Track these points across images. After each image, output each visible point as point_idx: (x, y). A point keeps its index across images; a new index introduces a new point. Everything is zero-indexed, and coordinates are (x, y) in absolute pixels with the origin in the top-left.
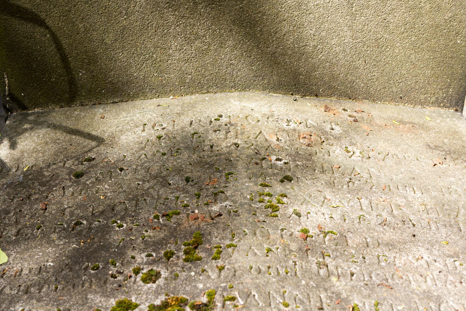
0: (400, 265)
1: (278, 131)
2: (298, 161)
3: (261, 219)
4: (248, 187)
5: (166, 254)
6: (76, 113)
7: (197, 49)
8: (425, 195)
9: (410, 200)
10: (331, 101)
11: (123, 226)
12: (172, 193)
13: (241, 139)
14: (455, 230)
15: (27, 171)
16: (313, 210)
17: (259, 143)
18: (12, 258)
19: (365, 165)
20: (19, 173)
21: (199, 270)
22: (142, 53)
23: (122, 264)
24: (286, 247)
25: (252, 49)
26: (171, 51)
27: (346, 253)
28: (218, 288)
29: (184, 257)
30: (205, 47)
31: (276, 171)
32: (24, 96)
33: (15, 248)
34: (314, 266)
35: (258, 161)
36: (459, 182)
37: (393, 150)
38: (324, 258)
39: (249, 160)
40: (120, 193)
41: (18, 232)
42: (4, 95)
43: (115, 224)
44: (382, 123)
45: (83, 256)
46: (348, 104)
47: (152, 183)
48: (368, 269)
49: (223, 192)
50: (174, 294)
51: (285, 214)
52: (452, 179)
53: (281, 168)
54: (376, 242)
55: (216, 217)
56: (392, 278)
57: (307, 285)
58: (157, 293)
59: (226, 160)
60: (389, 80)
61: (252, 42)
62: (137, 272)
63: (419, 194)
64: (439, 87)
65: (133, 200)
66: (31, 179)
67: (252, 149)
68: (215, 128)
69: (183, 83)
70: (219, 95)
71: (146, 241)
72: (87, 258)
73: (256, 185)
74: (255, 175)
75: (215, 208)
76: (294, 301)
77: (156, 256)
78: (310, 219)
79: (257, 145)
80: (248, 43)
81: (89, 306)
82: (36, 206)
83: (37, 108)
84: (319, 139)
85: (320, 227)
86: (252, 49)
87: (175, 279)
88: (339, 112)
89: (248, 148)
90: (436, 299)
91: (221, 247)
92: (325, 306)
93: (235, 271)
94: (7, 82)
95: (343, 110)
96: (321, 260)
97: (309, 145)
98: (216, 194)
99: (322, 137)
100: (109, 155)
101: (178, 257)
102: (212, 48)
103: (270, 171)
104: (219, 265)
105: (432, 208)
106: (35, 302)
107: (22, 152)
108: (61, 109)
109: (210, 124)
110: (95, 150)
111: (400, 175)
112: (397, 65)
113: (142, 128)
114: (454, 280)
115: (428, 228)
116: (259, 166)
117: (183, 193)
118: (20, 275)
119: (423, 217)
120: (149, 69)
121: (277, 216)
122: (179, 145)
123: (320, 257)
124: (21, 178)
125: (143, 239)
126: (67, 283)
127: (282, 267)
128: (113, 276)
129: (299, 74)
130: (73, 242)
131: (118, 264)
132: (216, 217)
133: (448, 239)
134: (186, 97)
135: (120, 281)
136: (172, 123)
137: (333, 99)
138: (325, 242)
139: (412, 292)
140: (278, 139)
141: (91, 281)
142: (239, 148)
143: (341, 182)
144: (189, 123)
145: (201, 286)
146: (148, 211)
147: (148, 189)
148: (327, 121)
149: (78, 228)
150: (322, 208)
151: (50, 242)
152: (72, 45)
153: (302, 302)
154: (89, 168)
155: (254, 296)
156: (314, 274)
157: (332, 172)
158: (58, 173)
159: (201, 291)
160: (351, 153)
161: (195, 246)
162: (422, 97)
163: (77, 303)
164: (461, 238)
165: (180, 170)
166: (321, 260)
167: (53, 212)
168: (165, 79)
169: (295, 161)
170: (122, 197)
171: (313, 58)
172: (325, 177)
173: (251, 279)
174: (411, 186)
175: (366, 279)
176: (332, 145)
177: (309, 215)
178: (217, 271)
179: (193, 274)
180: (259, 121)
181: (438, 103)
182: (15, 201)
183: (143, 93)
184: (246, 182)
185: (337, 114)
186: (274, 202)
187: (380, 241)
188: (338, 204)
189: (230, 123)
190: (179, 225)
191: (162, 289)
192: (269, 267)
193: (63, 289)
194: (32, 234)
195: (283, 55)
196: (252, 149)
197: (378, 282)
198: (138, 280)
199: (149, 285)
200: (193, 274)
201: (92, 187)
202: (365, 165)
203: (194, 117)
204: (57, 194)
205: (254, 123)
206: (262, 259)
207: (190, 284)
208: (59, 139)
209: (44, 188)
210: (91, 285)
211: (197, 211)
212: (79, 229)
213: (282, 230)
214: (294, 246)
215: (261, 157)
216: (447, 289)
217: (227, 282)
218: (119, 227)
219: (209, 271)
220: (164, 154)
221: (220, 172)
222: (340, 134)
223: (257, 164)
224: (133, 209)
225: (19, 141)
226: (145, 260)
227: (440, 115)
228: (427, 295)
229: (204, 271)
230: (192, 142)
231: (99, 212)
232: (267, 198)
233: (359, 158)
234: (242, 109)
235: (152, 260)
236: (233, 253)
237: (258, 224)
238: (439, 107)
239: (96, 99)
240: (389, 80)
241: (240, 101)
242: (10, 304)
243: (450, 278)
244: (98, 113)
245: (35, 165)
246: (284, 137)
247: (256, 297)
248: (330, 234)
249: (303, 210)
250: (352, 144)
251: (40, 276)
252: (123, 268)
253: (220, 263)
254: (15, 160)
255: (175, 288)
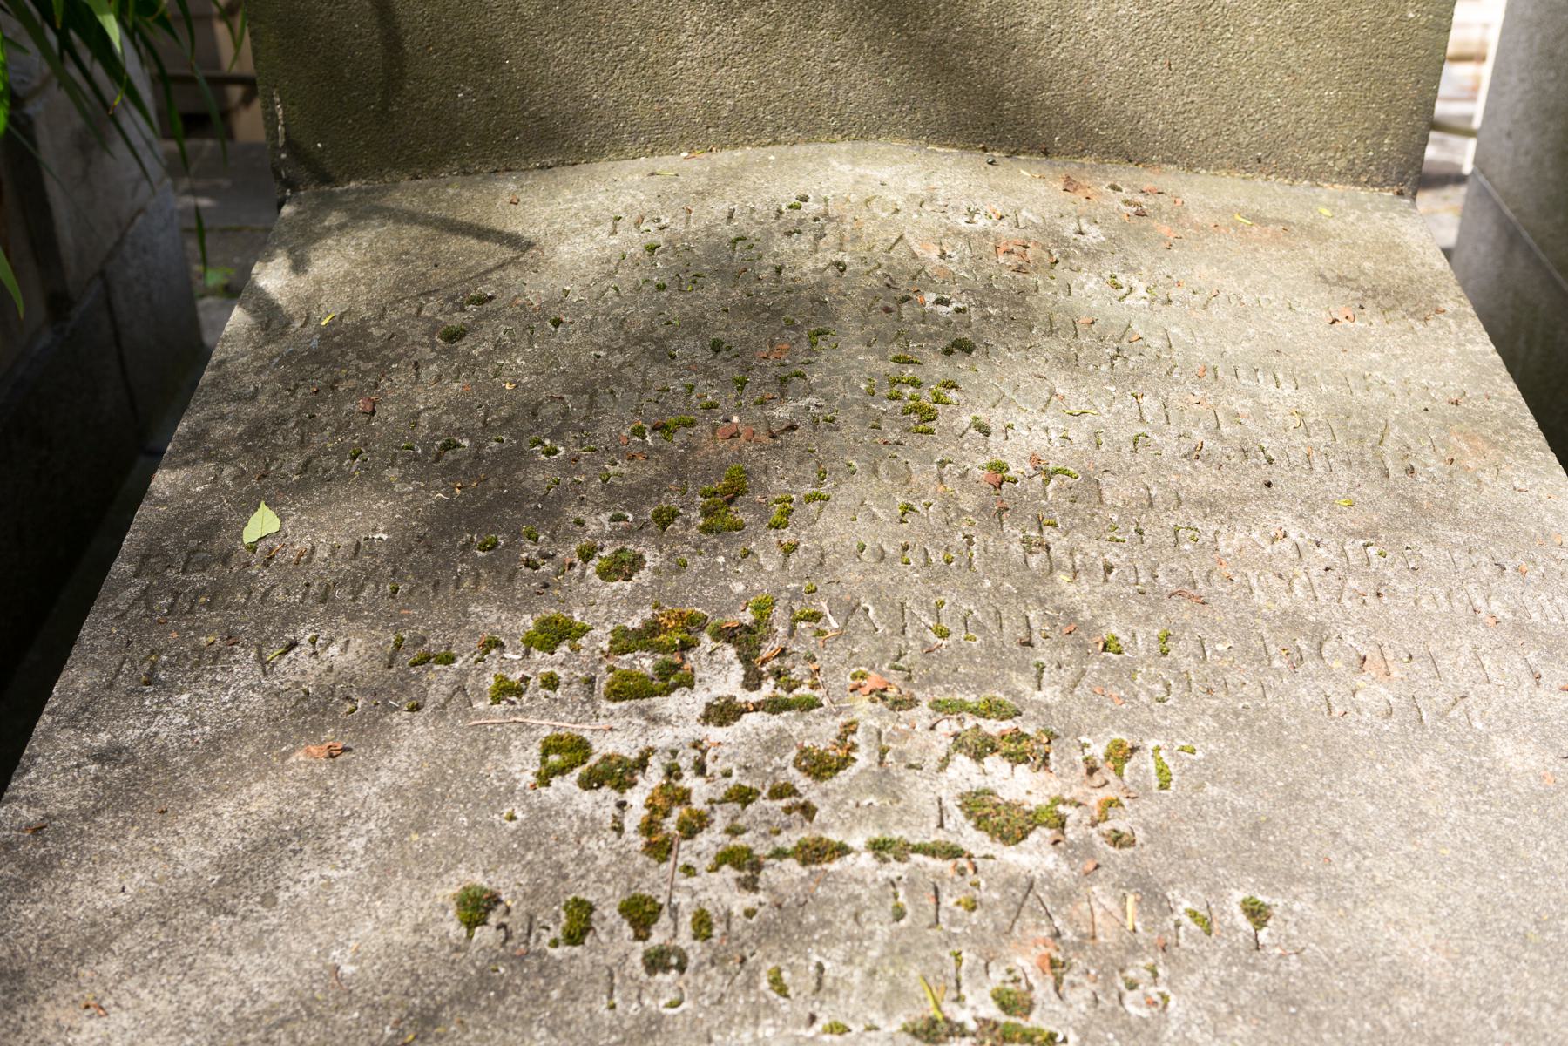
0: (1230, 550)
1: (945, 236)
2: (991, 305)
3: (892, 436)
4: (863, 364)
5: (658, 516)
6: (451, 191)
7: (749, 32)
8: (1303, 391)
9: (1265, 401)
10: (1083, 166)
11: (556, 452)
12: (677, 377)
13: (851, 253)
14: (1374, 474)
15: (329, 325)
16: (1021, 419)
17: (895, 262)
18: (290, 522)
19: (1158, 319)
20: (310, 329)
21: (737, 551)
22: (611, 42)
23: (553, 537)
24: (949, 502)
25: (885, 33)
26: (683, 37)
27: (1096, 519)
28: (780, 591)
29: (701, 522)
30: (768, 27)
31: (935, 328)
32: (324, 148)
33: (299, 500)
34: (1016, 548)
35: (891, 305)
36: (1394, 363)
37: (1230, 285)
38: (1041, 530)
39: (870, 301)
40: (551, 376)
41: (305, 465)
42: (275, 147)
43: (538, 448)
44: (1209, 220)
45: (459, 519)
46: (1126, 175)
47: (629, 354)
48: (1149, 556)
49: (801, 376)
50: (674, 604)
51: (952, 428)
52: (1374, 356)
53: (948, 322)
54: (1172, 497)
55: (782, 432)
56: (1208, 580)
57: (997, 589)
58: (634, 602)
59: (813, 301)
60: (1230, 112)
61: (886, 14)
62: (587, 555)
63: (1288, 389)
64: (1357, 132)
65: (583, 392)
66: (339, 345)
67: (877, 277)
68: (789, 228)
69: (712, 118)
70: (801, 149)
71: (611, 485)
72: (469, 523)
73: (884, 359)
74: (881, 336)
75: (782, 412)
76: (961, 625)
77: (635, 520)
78: (1013, 440)
79: (890, 268)
80: (875, 18)
81: (471, 631)
82: (349, 406)
83: (356, 179)
84: (1046, 256)
85: (1035, 460)
86: (885, 33)
87: (678, 572)
88: (1101, 194)
89: (868, 273)
90: (1314, 631)
91: (791, 501)
92: (1037, 638)
93: (822, 556)
94: (280, 113)
95: (1109, 192)
96: (1034, 534)
97: (1018, 270)
98: (784, 380)
99: (1054, 251)
100: (527, 289)
101: (687, 522)
102: (784, 29)
103: (919, 327)
104: (784, 540)
105: (1318, 423)
106: (344, 621)
107: (319, 282)
108: (415, 183)
109: (778, 218)
110: (494, 276)
111: (1245, 344)
112: (1251, 75)
113: (609, 226)
114: (1361, 590)
115: (1306, 467)
116: (893, 315)
117: (706, 378)
118: (309, 561)
119: (1295, 442)
120: (628, 82)
121: (931, 432)
122: (698, 266)
123: (1032, 528)
124: (315, 342)
125: (604, 481)
126: (421, 578)
127: (938, 547)
128: (529, 563)
129: (1003, 98)
130: (437, 488)
131: (542, 537)
132: (782, 432)
133: (1353, 494)
134: (720, 155)
135: (547, 574)
136: (684, 216)
137: (1087, 161)
138: (1045, 494)
139: (1253, 613)
140: (943, 255)
141: (479, 575)
142: (846, 274)
143: (1096, 358)
144: (725, 216)
145: (739, 587)
146: (619, 417)
147: (620, 367)
148: (1069, 214)
149: (450, 456)
150: (1044, 416)
151: (382, 487)
152: (438, 21)
153: (981, 628)
154: (479, 319)
155: (867, 610)
156: (1016, 564)
157: (1072, 333)
158: (404, 331)
159: (739, 597)
160: (1125, 290)
161: (727, 502)
162: (1314, 158)
163: (444, 624)
164: (1388, 494)
165: (699, 325)
166: (1034, 534)
167: (391, 419)
168: (669, 109)
169: (982, 305)
170: (556, 386)
171: (1037, 57)
172: (1056, 345)
173: (861, 572)
174: (1271, 370)
175: (1142, 581)
176: (1079, 270)
177: (1010, 432)
178: (779, 553)
179: (721, 559)
180: (897, 211)
181: (1353, 175)
182: (300, 394)
183: (615, 143)
184: (859, 352)
185: (1094, 199)
186: (926, 399)
187: (1182, 495)
188: (1084, 407)
189: (826, 215)
190: (693, 449)
191: (645, 593)
192: (906, 548)
193: (411, 592)
194: (339, 469)
195: (963, 47)
196: (877, 277)
197: (1172, 588)
198: (588, 572)
199: (615, 585)
200: (721, 559)
201: (486, 363)
202: (1158, 319)
203: (739, 202)
204: (400, 380)
205: (885, 215)
206: (890, 528)
207: (712, 584)
208: (407, 253)
209: (370, 366)
210: (477, 585)
211: (735, 419)
212: (452, 458)
213: (942, 464)
214: (968, 501)
215: (898, 296)
216: (1344, 608)
217: (802, 580)
218: (548, 453)
219: (761, 553)
220: (661, 288)
221: (796, 328)
222: (1098, 244)
223: (887, 310)
224: (583, 412)
225: (312, 255)
226: (608, 528)
227: (1358, 205)
228: (1292, 621)
229: (747, 554)
230: (731, 259)
231: (500, 419)
232: (908, 391)
233: (1143, 302)
234: (857, 182)
235: (624, 529)
236: (819, 513)
237: (885, 449)
238: (1356, 183)
239: (499, 159)
240: (1230, 112)
241: (853, 163)
242: (285, 625)
243: (1352, 583)
244: (505, 192)
245: (349, 312)
246: (957, 249)
247: (871, 613)
248: (1061, 476)
249: (996, 419)
250: (1128, 269)
251: (357, 563)
252: (554, 546)
253: (788, 536)
254: (300, 300)
255: (676, 591)
